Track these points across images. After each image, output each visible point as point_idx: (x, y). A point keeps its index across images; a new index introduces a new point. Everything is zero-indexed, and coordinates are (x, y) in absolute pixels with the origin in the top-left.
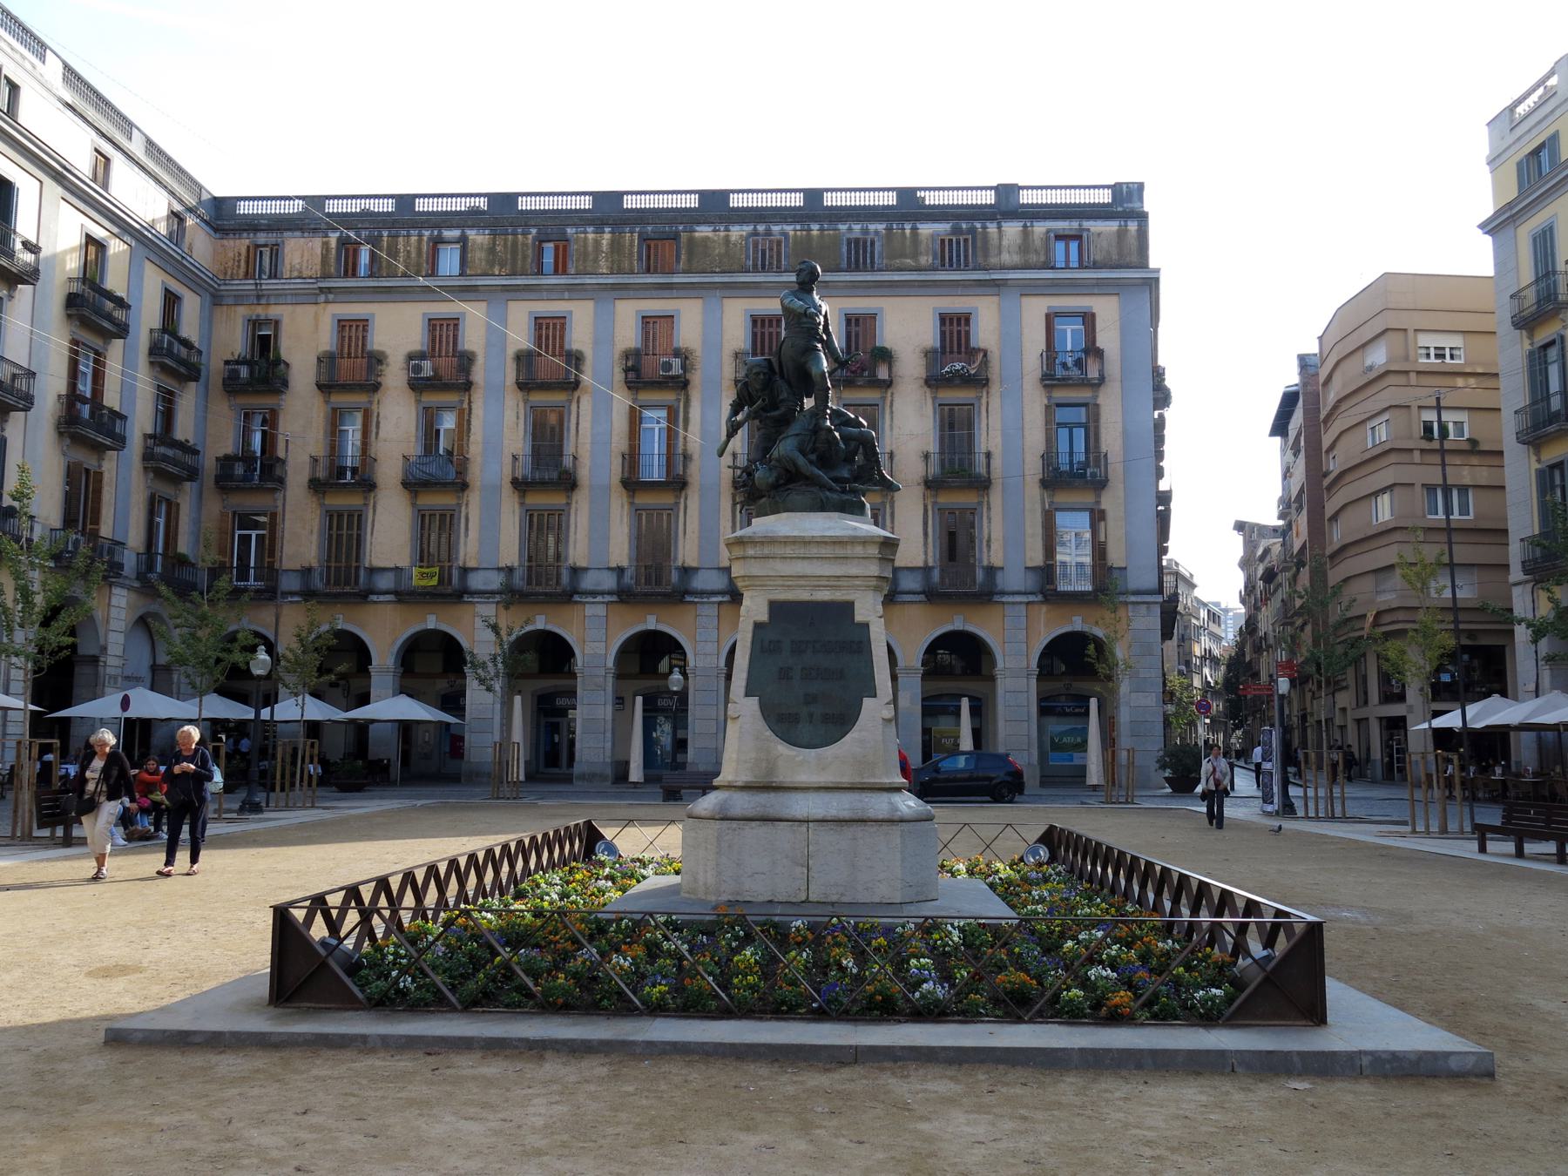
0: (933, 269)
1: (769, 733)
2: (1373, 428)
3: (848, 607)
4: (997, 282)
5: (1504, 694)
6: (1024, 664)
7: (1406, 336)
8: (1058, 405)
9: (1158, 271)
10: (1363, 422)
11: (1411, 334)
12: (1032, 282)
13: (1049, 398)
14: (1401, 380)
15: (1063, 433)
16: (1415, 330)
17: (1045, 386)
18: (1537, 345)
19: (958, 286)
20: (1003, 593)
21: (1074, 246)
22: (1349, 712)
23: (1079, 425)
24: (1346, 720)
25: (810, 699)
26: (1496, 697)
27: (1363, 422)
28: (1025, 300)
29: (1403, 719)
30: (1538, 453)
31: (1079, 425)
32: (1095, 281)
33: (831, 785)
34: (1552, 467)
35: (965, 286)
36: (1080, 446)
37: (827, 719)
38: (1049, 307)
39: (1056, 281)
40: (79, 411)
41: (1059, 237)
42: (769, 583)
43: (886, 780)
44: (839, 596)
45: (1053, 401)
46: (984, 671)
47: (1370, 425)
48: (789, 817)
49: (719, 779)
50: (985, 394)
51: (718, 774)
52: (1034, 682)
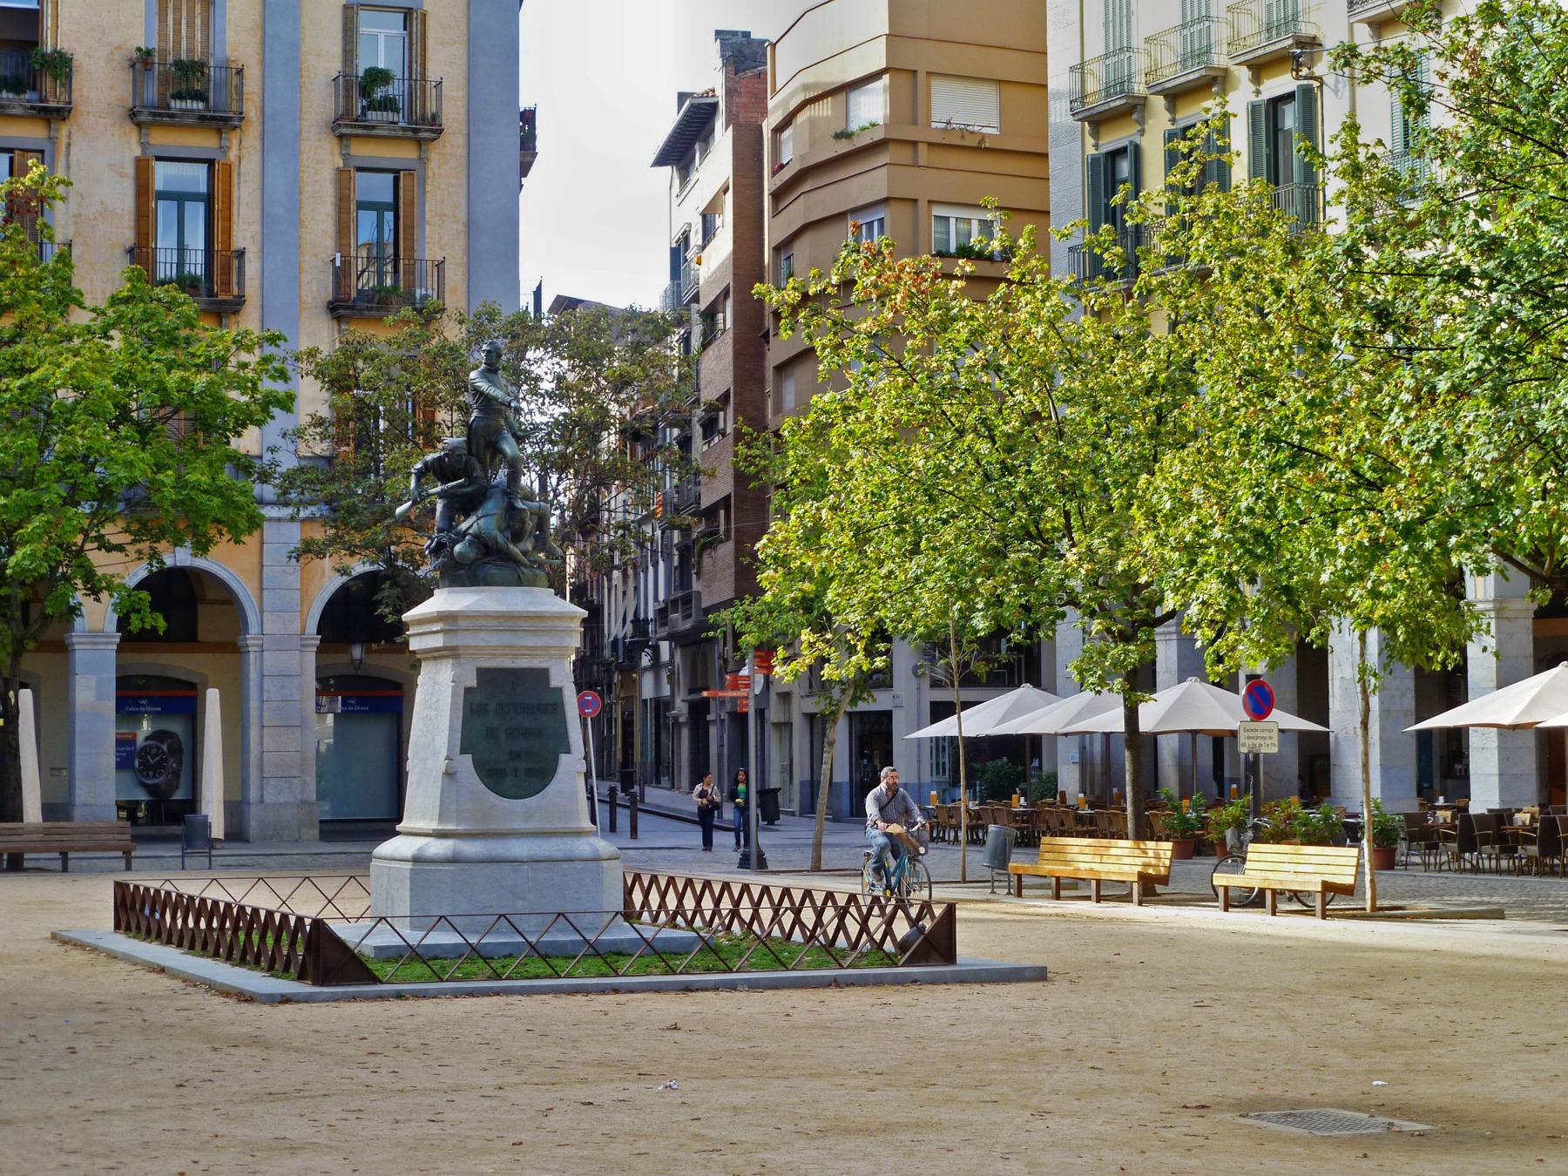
3: (544, 674)
5: (1037, 684)
6: (297, 627)
7: (915, 83)
8: (360, 169)
10: (841, 216)
11: (921, 77)
13: (346, 157)
14: (904, 154)
15: (165, 213)
17: (341, 137)
18: (1104, 149)
22: (795, 699)
24: (789, 712)
25: (515, 756)
26: (1026, 689)
29: (886, 716)
30: (1095, 134)
31: (195, 197)
34: (1115, 155)
36: (196, 239)
37: (529, 772)
43: (571, 825)
44: (536, 663)
45: (152, 152)
46: (205, 631)
50: (235, 142)
51: (400, 820)
52: (311, 659)
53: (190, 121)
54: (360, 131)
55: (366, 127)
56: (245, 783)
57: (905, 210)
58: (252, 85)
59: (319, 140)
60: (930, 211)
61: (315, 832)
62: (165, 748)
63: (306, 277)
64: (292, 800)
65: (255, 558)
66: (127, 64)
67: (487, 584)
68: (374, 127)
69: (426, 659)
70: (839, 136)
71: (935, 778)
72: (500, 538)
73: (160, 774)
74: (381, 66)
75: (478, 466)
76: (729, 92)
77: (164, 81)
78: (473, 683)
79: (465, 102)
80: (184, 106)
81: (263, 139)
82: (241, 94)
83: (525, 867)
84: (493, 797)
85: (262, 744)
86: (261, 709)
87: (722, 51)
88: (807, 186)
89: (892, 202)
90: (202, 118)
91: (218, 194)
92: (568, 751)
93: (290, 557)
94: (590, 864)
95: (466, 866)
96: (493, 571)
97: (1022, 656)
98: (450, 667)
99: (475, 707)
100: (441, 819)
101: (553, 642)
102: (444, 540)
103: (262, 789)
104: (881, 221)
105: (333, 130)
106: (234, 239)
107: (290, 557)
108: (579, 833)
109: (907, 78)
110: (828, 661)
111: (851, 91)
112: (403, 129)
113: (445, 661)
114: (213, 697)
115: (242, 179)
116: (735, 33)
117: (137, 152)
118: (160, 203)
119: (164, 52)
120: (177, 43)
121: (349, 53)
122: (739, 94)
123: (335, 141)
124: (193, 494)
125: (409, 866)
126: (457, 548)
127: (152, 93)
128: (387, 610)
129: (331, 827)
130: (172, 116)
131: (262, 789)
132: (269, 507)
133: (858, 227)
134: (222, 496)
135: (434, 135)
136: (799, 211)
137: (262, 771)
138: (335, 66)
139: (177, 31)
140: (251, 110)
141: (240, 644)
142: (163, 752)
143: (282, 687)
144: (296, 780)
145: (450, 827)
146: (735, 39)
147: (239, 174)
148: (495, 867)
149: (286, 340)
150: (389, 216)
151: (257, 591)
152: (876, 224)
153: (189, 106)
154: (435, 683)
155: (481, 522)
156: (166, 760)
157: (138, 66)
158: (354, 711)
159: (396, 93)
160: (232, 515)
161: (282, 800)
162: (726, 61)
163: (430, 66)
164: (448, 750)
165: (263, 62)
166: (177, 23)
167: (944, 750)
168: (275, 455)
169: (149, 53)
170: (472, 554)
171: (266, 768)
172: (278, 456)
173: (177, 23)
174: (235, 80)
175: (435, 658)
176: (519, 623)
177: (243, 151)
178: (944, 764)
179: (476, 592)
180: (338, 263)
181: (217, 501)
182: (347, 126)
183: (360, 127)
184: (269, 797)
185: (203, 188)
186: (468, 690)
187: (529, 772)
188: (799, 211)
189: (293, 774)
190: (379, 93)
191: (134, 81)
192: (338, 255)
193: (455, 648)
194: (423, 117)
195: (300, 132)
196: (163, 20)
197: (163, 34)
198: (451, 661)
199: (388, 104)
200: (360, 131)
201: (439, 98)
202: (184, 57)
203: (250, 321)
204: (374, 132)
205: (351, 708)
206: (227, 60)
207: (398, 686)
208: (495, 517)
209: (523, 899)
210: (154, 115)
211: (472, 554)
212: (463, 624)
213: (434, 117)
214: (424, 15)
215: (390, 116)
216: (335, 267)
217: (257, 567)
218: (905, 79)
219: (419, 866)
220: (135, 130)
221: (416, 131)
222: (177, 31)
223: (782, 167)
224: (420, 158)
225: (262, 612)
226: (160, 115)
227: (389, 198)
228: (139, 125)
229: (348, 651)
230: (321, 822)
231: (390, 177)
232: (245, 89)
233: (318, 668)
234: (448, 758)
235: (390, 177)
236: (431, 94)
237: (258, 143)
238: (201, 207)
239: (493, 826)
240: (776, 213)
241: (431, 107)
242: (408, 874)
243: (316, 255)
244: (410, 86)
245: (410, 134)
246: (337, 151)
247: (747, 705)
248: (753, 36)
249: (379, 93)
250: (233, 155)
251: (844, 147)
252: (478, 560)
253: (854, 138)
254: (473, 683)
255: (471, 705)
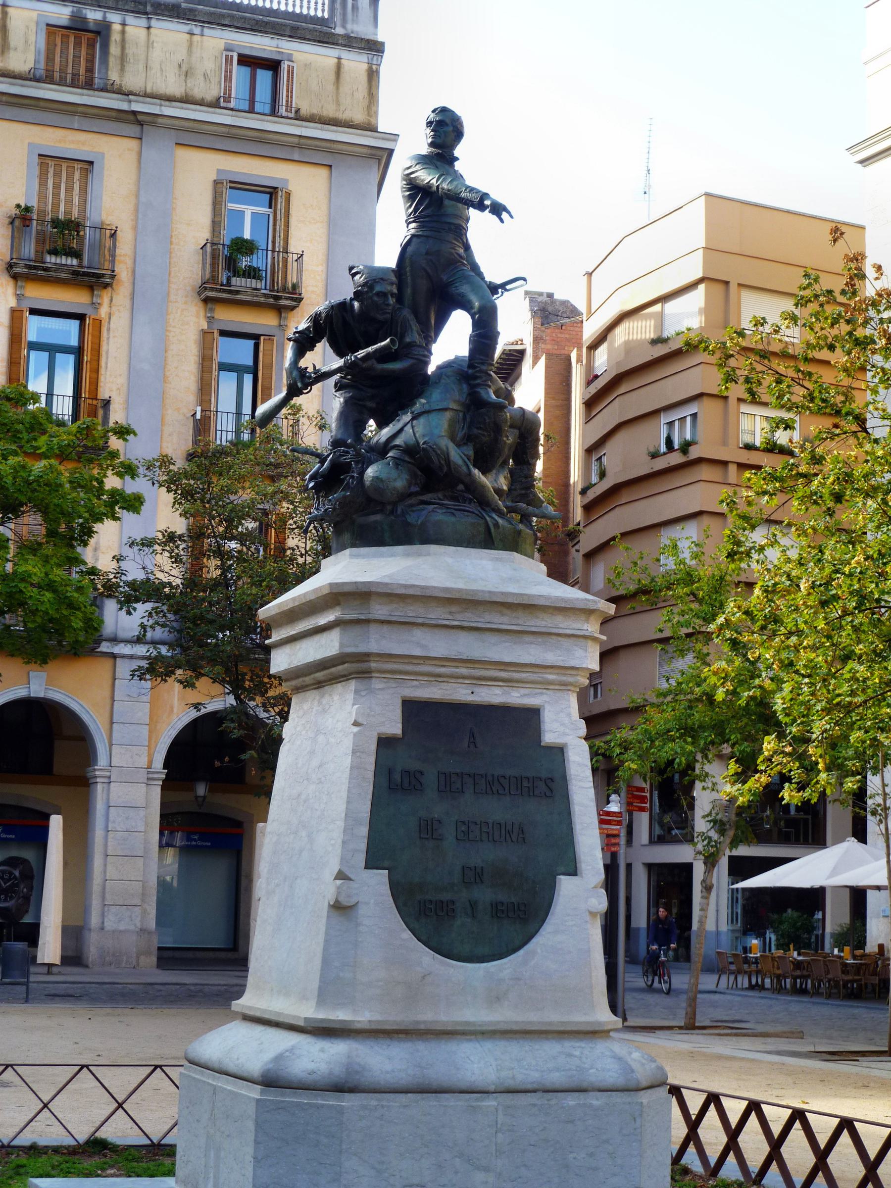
0: (32, 77)
1: (407, 935)
2: (671, 424)
3: (532, 715)
4: (140, 117)
6: (143, 761)
8: (224, 333)
9: (394, 137)
10: (656, 413)
11: (733, 287)
12: (196, 125)
13: (210, 320)
15: (37, 361)
16: (739, 285)
17: (206, 301)
19: (74, 113)
20: (115, 640)
21: (264, 77)
23: (65, 350)
27: (656, 413)
28: (182, 153)
31: (65, 350)
32: (296, 140)
33: (515, 1028)
35: (85, 115)
36: (65, 385)
37: (498, 911)
38: (219, 171)
39: (234, 131)
40: (484, 396)
41: (246, 60)
42: (524, 675)
43: (579, 1018)
44: (516, 697)
45: (26, 305)
46: (60, 766)
47: (664, 419)
48: (463, 1085)
49: (240, 1001)
50: (106, 300)
51: (239, 994)
52: (156, 792)
53: (63, 275)
54: (225, 295)
55: (230, 292)
56: (86, 910)
57: (717, 404)
58: (124, 247)
59: (186, 303)
60: (738, 409)
61: (154, 959)
62: (17, 873)
63: (167, 430)
64: (132, 927)
65: (107, 693)
66: (7, 221)
67: (426, 540)
68: (238, 292)
69: (298, 689)
70: (655, 342)
71: (730, 928)
72: (456, 455)
73: (12, 898)
74: (247, 235)
75: (415, 327)
76: (537, 340)
77: (41, 239)
78: (395, 728)
79: (324, 276)
80: (58, 261)
81: (132, 299)
82: (113, 256)
83: (491, 1102)
84: (427, 958)
85: (105, 872)
86: (106, 838)
87: (530, 306)
88: (623, 389)
89: (705, 399)
90: (75, 273)
91: (88, 346)
92: (574, 872)
93: (133, 675)
94: (617, 1098)
95: (371, 1100)
96: (439, 516)
97: (810, 817)
98: (350, 696)
99: (397, 777)
100: (323, 998)
101: (551, 657)
102: (347, 458)
103: (103, 915)
104: (694, 416)
105: (199, 294)
106: (100, 390)
107: (133, 675)
108: (594, 1033)
109: (720, 288)
110: (789, 780)
111: (665, 302)
112: (265, 295)
113: (339, 687)
114: (56, 823)
115: (111, 335)
116: (541, 294)
117: (13, 303)
118: (33, 354)
119: (42, 213)
120: (56, 205)
121: (216, 225)
122: (545, 342)
123: (201, 304)
124: (22, 586)
125: (255, 1092)
126: (371, 472)
127: (29, 249)
128: (232, 725)
129: (169, 954)
130: (46, 269)
131: (103, 915)
132: (122, 645)
133: (671, 424)
134: (55, 591)
135: (294, 303)
136: (609, 417)
137: (103, 898)
138: (204, 234)
139: (56, 195)
140: (123, 271)
141: (89, 775)
142: (15, 877)
143: (127, 818)
144: (137, 909)
145: (341, 1015)
146: (540, 299)
147: (109, 330)
148: (430, 1102)
149: (135, 434)
150: (248, 379)
151: (107, 726)
152: (689, 419)
153: (64, 262)
154: (318, 732)
155: (420, 426)
156: (17, 885)
157: (17, 223)
158: (197, 846)
159: (260, 265)
160: (65, 613)
161: (122, 927)
162: (534, 314)
163: (292, 242)
164: (343, 859)
165: (135, 228)
166: (57, 187)
167: (737, 901)
168: (122, 563)
169: (27, 209)
170: (399, 482)
171: (107, 896)
172: (124, 565)
173: (57, 187)
174: (108, 243)
175: (319, 685)
176: (487, 617)
177: (114, 308)
178: (737, 913)
179: (407, 555)
180: (198, 416)
181: (48, 595)
182: (212, 289)
183: (224, 291)
184: (109, 925)
185: (74, 342)
186: (385, 743)
187: (498, 911)
188: (609, 417)
189: (133, 903)
190: (244, 262)
191: (13, 237)
192: (199, 409)
193: (365, 657)
194: (284, 289)
195: (168, 294)
196: (43, 182)
197: (42, 196)
198: (352, 685)
199: (253, 273)
200: (225, 295)
201: (300, 271)
202: (61, 217)
203: (26, 142)
204: (239, 297)
205: (194, 843)
206: (102, 223)
207: (239, 824)
208: (448, 415)
209: (486, 1169)
210: (27, 266)
211: (399, 482)
212: (379, 610)
213: (295, 286)
214: (288, 195)
215: (254, 283)
216: (195, 420)
217: (108, 701)
218: (719, 289)
219: (273, 1096)
220: (11, 283)
221: (277, 298)
222: (56, 195)
223: (596, 377)
224: (280, 325)
225: (111, 745)
226: (35, 268)
227: (250, 362)
228: (15, 277)
229: (192, 789)
230: (159, 949)
231: (251, 343)
232: (118, 251)
233: (163, 805)
234: (341, 876)
235: (251, 343)
236: (292, 267)
237: (127, 302)
238: (71, 359)
239: (427, 1016)
240: (589, 418)
241: (292, 278)
242: (251, 1110)
243: (178, 409)
244: (273, 258)
245: (271, 301)
246: (202, 313)
247: (618, 844)
248: (555, 297)
249: (244, 262)
250: (103, 312)
251: (660, 351)
252: (411, 495)
253: (670, 342)
254: (395, 728)
255: (390, 772)
